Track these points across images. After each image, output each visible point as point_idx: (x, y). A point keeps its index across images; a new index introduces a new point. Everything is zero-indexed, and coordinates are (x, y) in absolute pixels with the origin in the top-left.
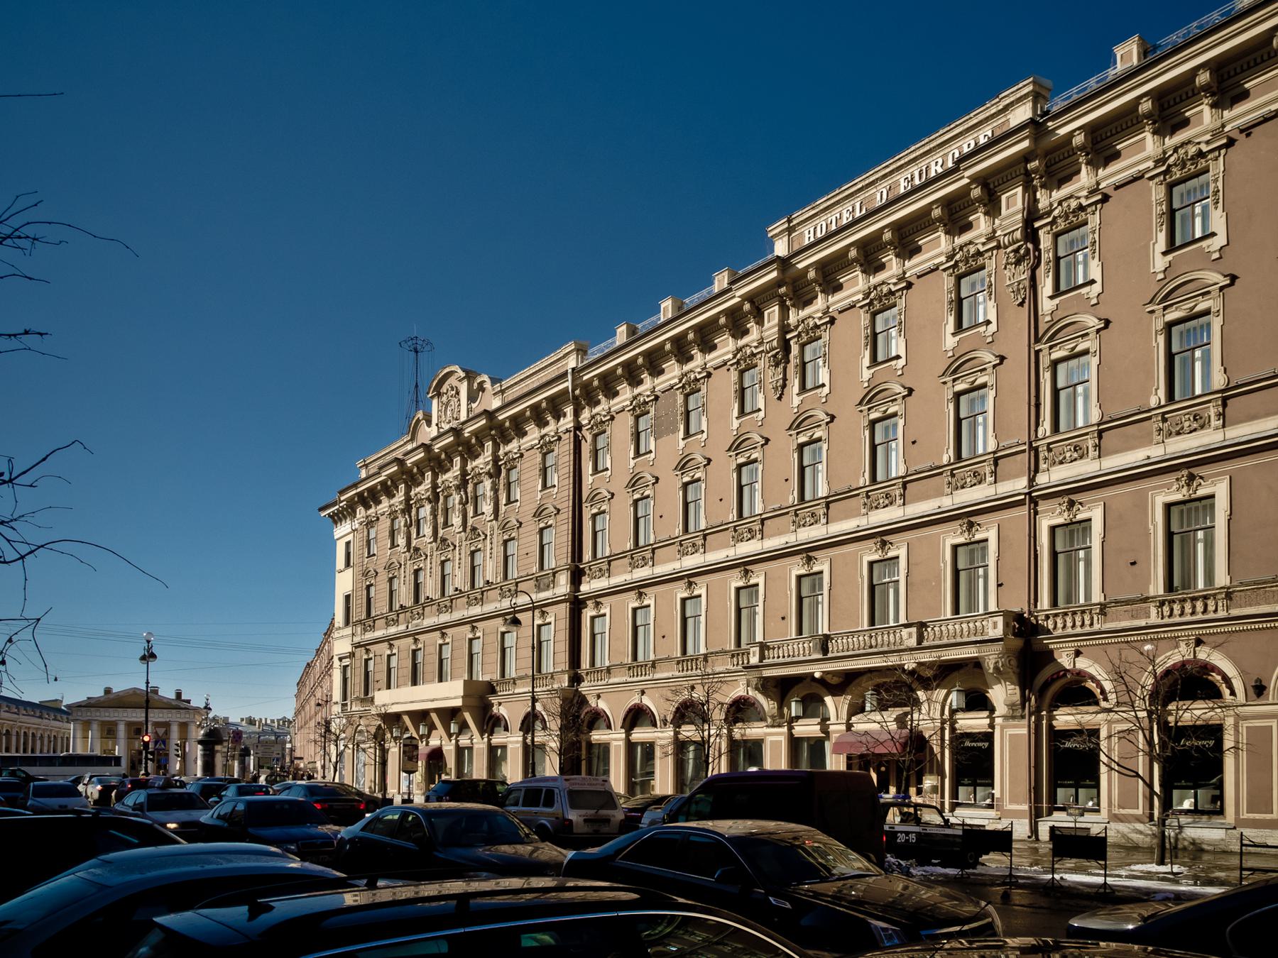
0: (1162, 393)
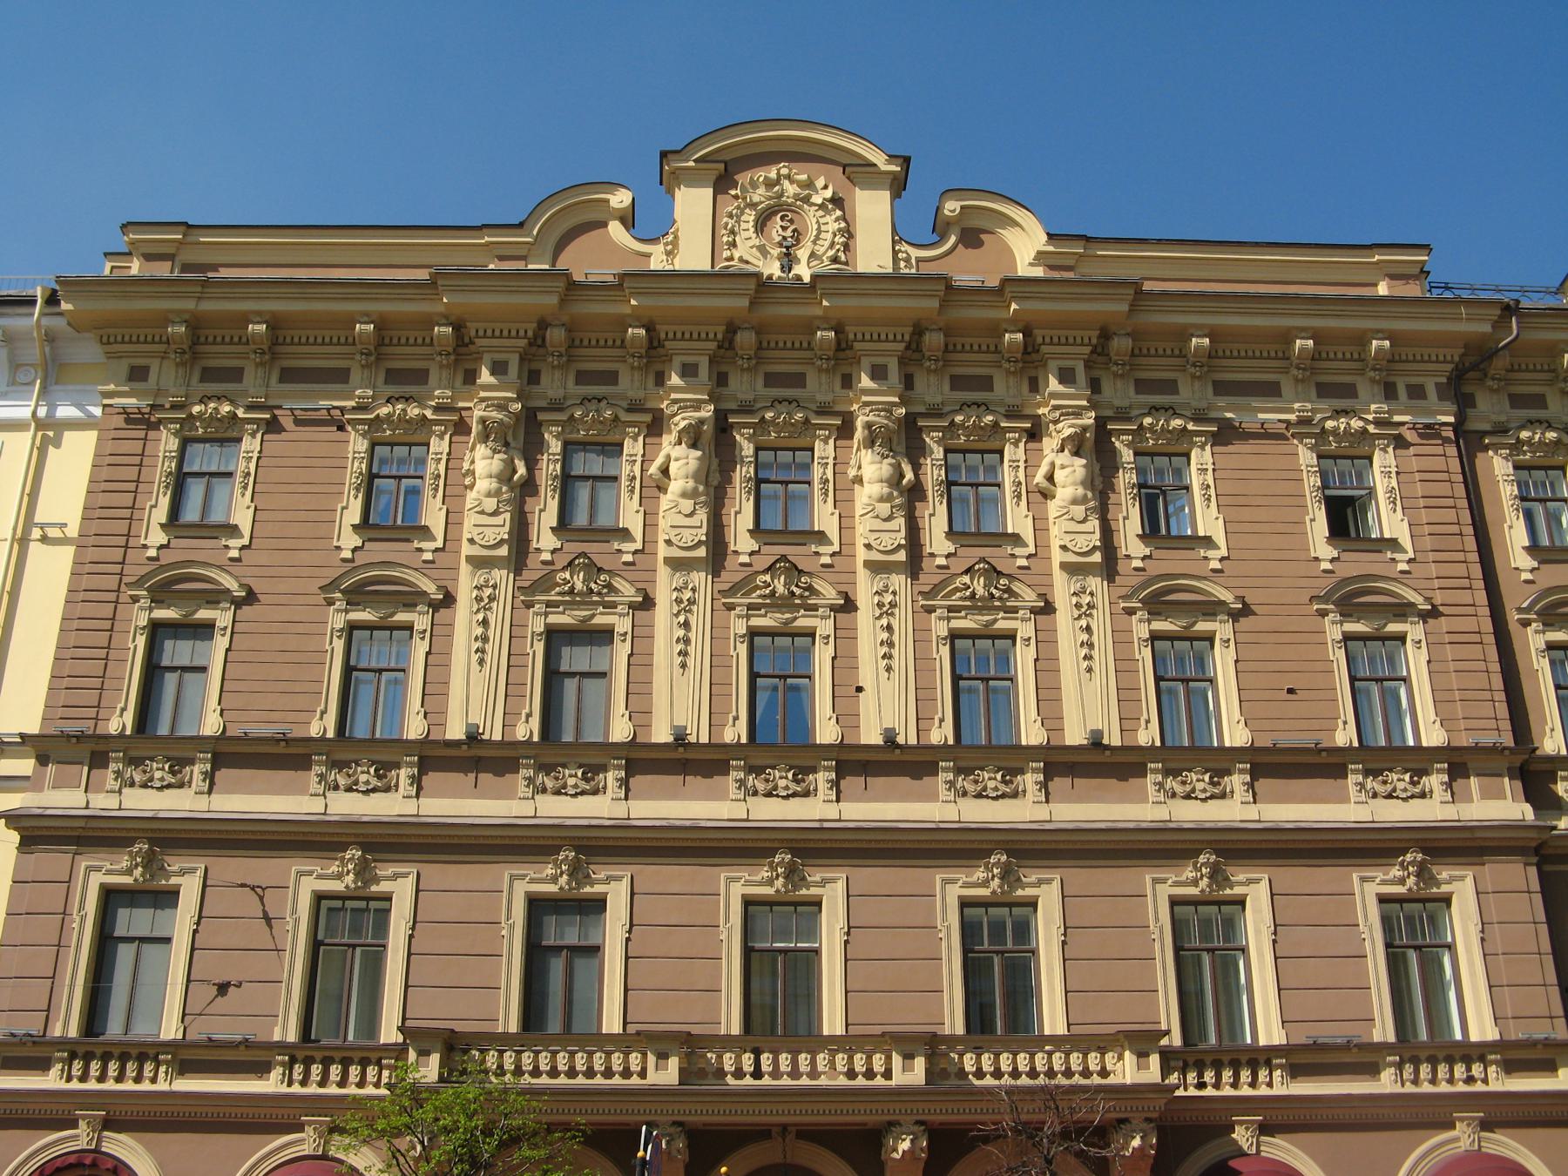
0: (129, 718)
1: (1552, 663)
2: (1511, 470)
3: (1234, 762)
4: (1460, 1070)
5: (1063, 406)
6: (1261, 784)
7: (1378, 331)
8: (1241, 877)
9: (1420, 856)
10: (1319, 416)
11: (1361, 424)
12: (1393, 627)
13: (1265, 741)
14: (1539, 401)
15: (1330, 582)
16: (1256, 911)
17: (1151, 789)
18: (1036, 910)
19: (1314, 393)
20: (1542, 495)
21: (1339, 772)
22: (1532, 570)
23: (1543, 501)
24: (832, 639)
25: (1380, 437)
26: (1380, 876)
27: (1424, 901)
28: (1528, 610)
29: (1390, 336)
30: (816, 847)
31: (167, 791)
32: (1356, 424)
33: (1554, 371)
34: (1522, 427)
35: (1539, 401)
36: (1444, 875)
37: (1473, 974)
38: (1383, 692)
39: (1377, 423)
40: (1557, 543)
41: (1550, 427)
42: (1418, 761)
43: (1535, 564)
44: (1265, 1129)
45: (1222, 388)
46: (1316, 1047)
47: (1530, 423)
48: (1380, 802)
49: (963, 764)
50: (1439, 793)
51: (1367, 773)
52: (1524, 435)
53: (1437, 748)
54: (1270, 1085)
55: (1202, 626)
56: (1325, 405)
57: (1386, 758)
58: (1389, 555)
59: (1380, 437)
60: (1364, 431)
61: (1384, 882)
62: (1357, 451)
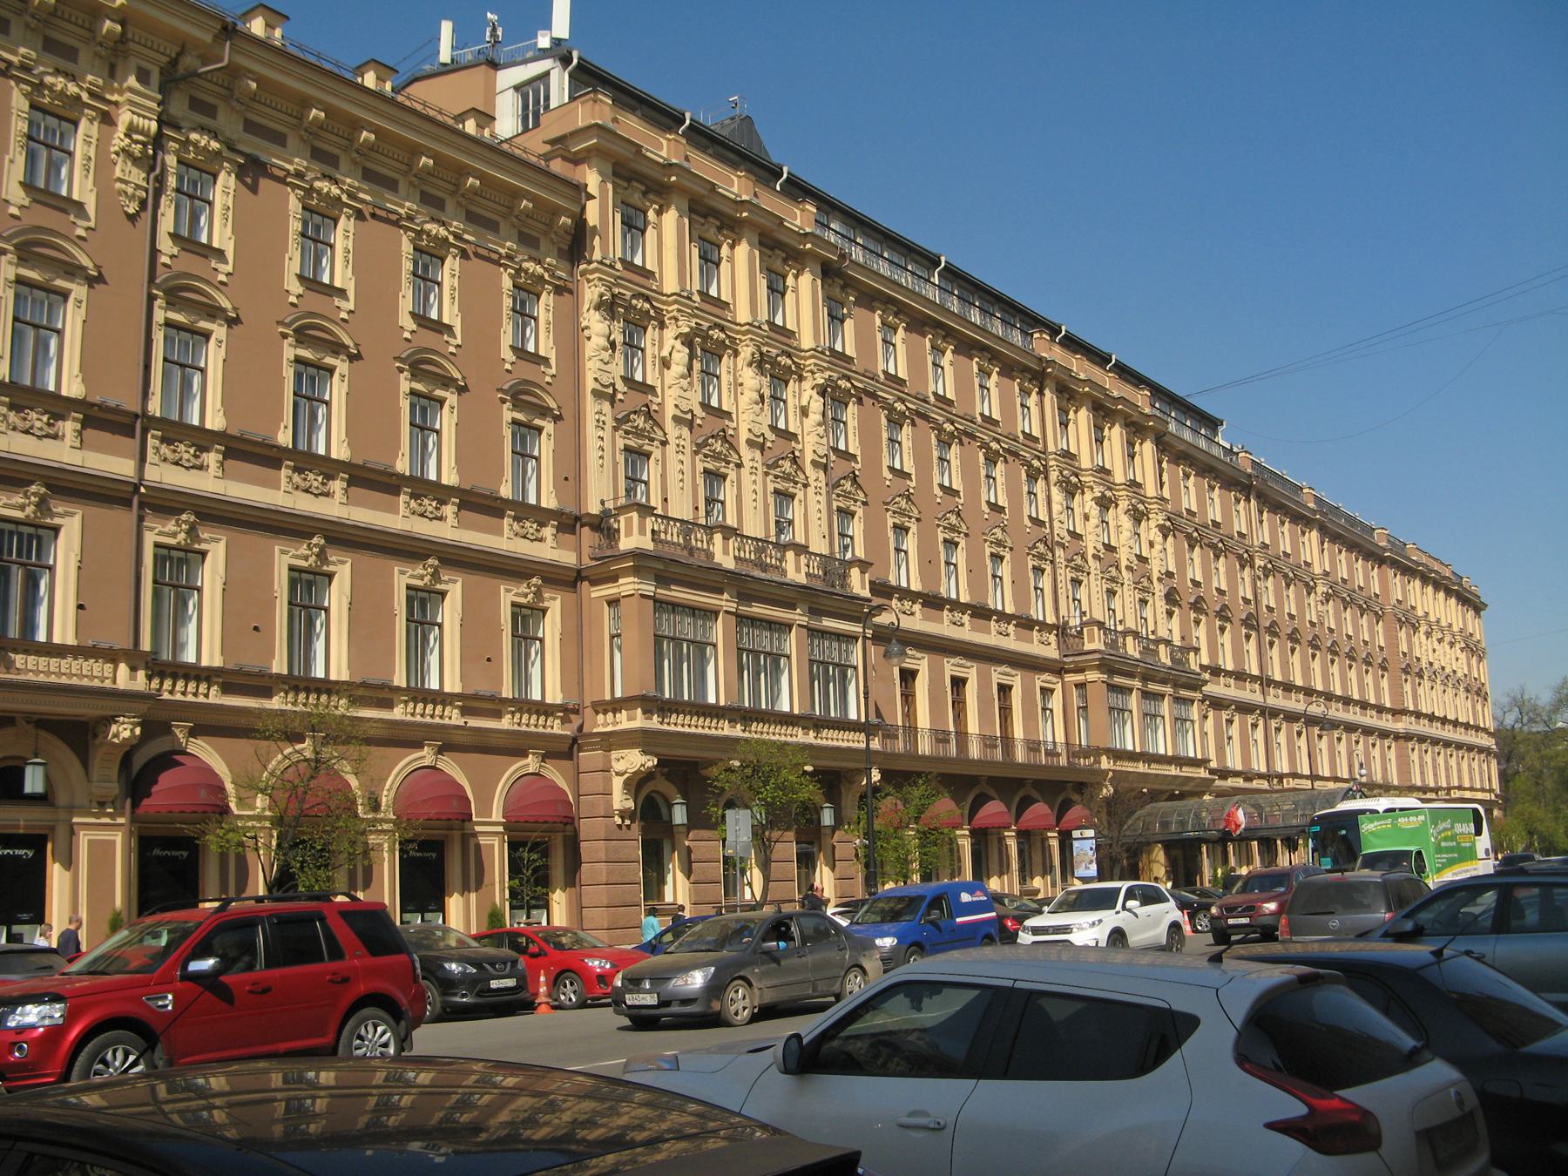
1: (17, 296)
2: (26, 108)
3: (70, 410)
4: (180, 685)
5: (135, 110)
6: (89, 432)
7: (320, 101)
8: (446, 578)
9: (43, 490)
10: (42, 69)
11: (76, 90)
12: (203, 324)
13: (234, 431)
14: (211, 111)
15: (16, 226)
16: (453, 600)
17: (284, 480)
18: (56, 537)
19: (40, 44)
20: (49, 141)
21: (275, 464)
22: (21, 207)
23: (49, 147)
24: (84, 305)
25: (549, 283)
26: (160, 528)
27: (37, 526)
28: (288, 325)
29: (376, 130)
30: (343, 537)
31: (45, 440)
32: (72, 89)
33: (90, 30)
34: (194, 130)
35: (211, 111)
36: (334, 558)
37: (340, 633)
38: (37, 338)
39: (92, 94)
40: (52, 189)
41: (216, 138)
42: (58, 407)
43: (26, 203)
44: (193, 733)
45: (250, 127)
46: (239, 672)
47: (202, 129)
48: (300, 494)
49: (18, 402)
50: (451, 519)
51: (296, 469)
52: (194, 136)
53: (343, 462)
54: (207, 696)
55: (203, 324)
56: (316, 166)
57: (306, 461)
58: (72, 218)
59: (549, 283)
60: (79, 97)
61: (161, 533)
62: (65, 114)
